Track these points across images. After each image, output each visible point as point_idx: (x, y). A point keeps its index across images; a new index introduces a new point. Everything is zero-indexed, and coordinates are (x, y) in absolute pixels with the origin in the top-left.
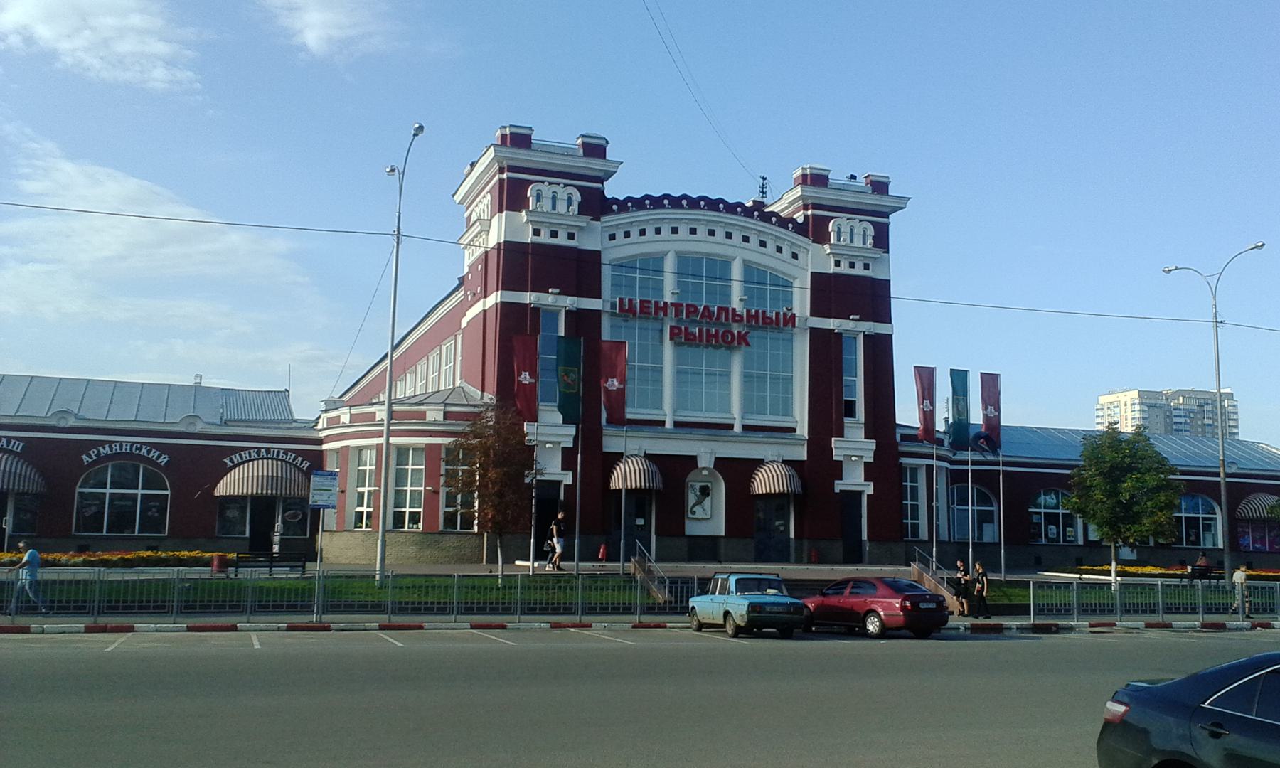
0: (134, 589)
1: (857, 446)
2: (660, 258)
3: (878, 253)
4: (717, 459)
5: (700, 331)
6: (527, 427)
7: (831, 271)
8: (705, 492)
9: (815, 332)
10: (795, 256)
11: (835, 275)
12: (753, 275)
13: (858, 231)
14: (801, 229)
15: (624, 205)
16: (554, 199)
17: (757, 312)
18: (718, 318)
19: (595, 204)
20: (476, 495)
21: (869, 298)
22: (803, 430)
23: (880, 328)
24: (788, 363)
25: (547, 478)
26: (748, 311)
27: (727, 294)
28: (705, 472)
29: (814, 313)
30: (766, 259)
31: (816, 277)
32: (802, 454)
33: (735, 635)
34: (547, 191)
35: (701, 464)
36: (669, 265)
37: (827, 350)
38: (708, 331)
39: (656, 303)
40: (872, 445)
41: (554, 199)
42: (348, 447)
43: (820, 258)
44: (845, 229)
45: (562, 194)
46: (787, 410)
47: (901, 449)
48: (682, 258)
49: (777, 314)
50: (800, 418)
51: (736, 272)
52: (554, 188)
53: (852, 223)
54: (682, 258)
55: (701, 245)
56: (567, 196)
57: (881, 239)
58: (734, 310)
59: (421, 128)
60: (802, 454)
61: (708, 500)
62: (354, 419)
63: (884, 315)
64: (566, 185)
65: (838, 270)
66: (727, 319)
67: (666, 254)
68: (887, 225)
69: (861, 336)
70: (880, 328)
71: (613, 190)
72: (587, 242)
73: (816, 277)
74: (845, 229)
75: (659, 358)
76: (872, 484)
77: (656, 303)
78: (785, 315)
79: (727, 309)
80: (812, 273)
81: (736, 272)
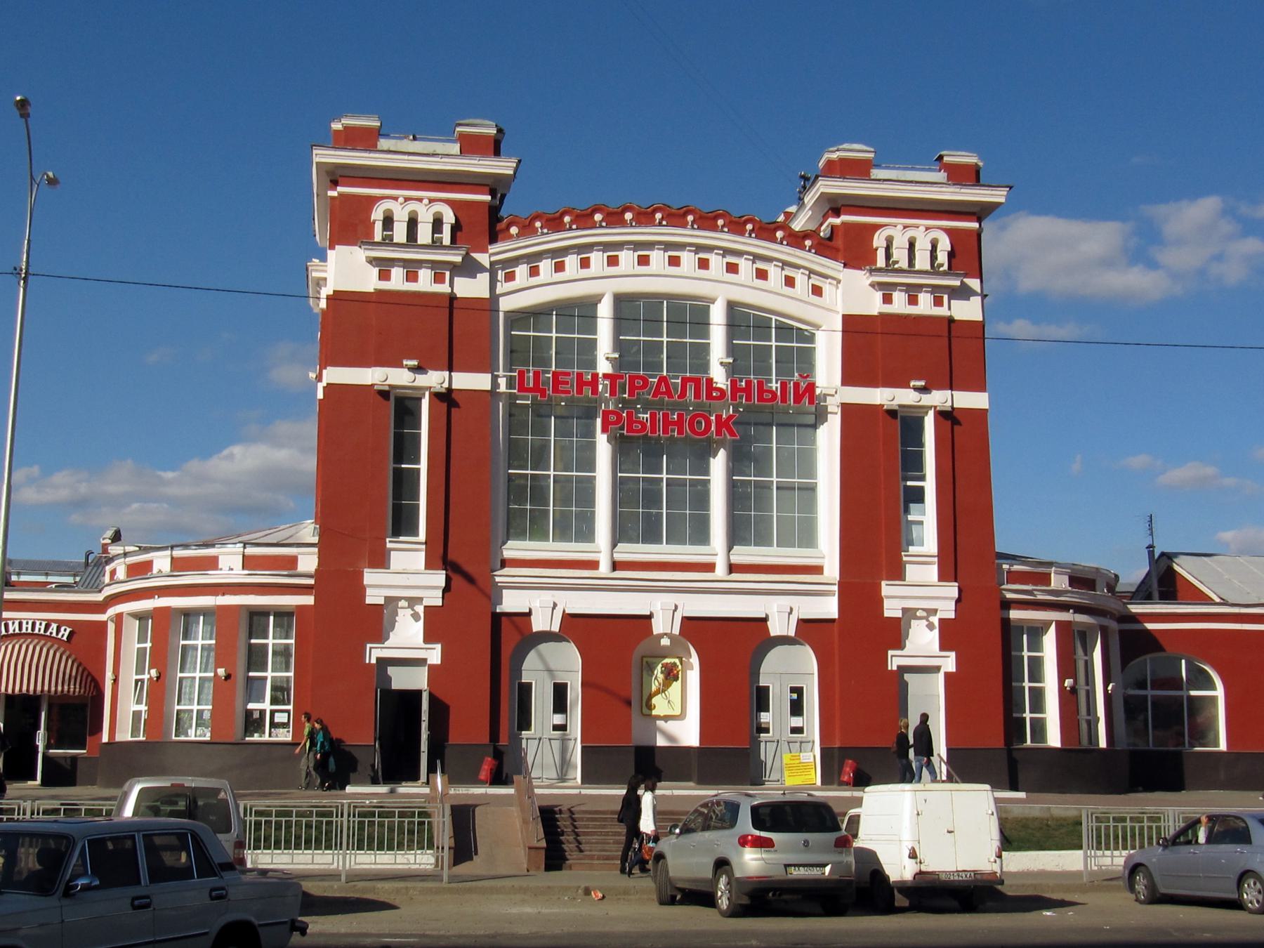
0: (411, 841)
1: (414, 580)
4: (686, 620)
5: (653, 416)
6: (371, 577)
8: (671, 675)
9: (849, 411)
10: (817, 291)
11: (883, 317)
13: (923, 247)
14: (825, 247)
17: (749, 383)
18: (683, 395)
22: (832, 570)
24: (807, 464)
26: (734, 383)
29: (849, 378)
30: (770, 296)
32: (829, 608)
33: (738, 911)
35: (658, 626)
38: (665, 416)
39: (580, 376)
40: (952, 590)
42: (168, 609)
43: (855, 293)
44: (900, 243)
48: (621, 301)
50: (827, 549)
51: (718, 315)
54: (621, 301)
60: (829, 608)
61: (676, 686)
62: (179, 565)
64: (431, 201)
65: (888, 309)
69: (931, 413)
74: (900, 243)
76: (953, 655)
77: (580, 376)
78: (797, 385)
79: (697, 382)
80: (844, 316)
81: (718, 315)
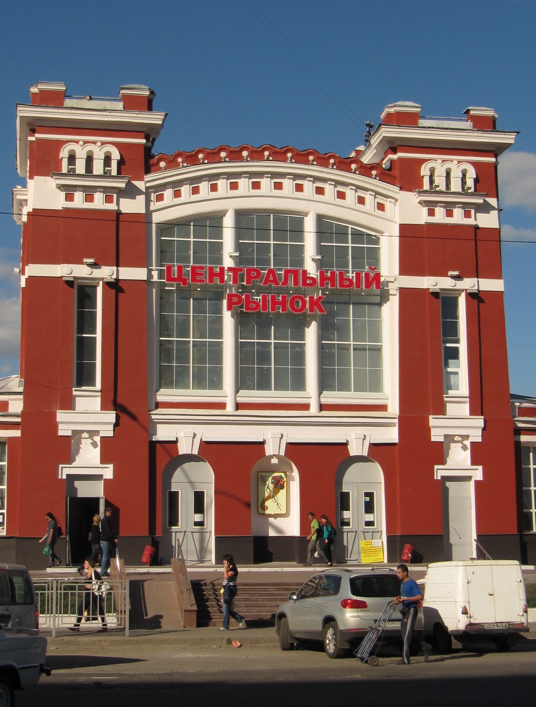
4: (290, 445)
5: (264, 298)
6: (61, 416)
7: (423, 222)
8: (279, 485)
10: (381, 207)
11: (429, 226)
12: (326, 228)
13: (456, 175)
16: (89, 160)
20: (192, 224)
22: (394, 408)
26: (322, 274)
27: (298, 252)
28: (274, 461)
30: (347, 211)
32: (391, 435)
35: (270, 450)
36: (229, 221)
38: (273, 298)
39: (211, 269)
46: (376, 384)
49: (358, 275)
50: (390, 392)
51: (310, 225)
53: (447, 165)
55: (267, 198)
58: (305, 272)
59: (492, 595)
60: (391, 435)
61: (282, 493)
66: (296, 283)
69: (463, 295)
75: (217, 331)
76: (480, 468)
77: (211, 269)
78: (367, 275)
79: (296, 273)
80: (400, 225)
81: (310, 225)
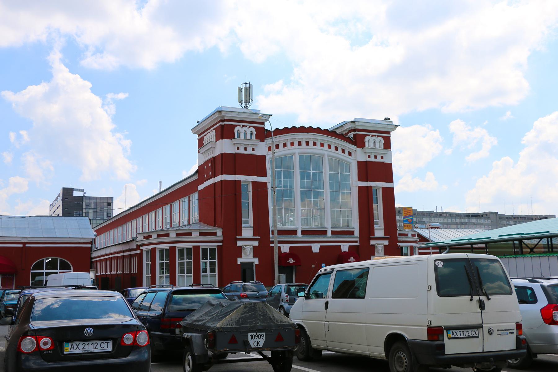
2: (292, 157)
3: (385, 151)
15: (278, 132)
19: (262, 134)
21: (384, 172)
23: (387, 185)
25: (446, 356)
31: (359, 163)
34: (242, 130)
37: (366, 196)
41: (245, 133)
43: (360, 155)
45: (249, 131)
47: (399, 239)
50: (355, 226)
52: (245, 128)
56: (251, 130)
57: (387, 145)
59: (160, 182)
63: (389, 178)
67: (294, 154)
68: (389, 137)
70: (387, 185)
71: (267, 126)
72: (258, 152)
73: (359, 163)
